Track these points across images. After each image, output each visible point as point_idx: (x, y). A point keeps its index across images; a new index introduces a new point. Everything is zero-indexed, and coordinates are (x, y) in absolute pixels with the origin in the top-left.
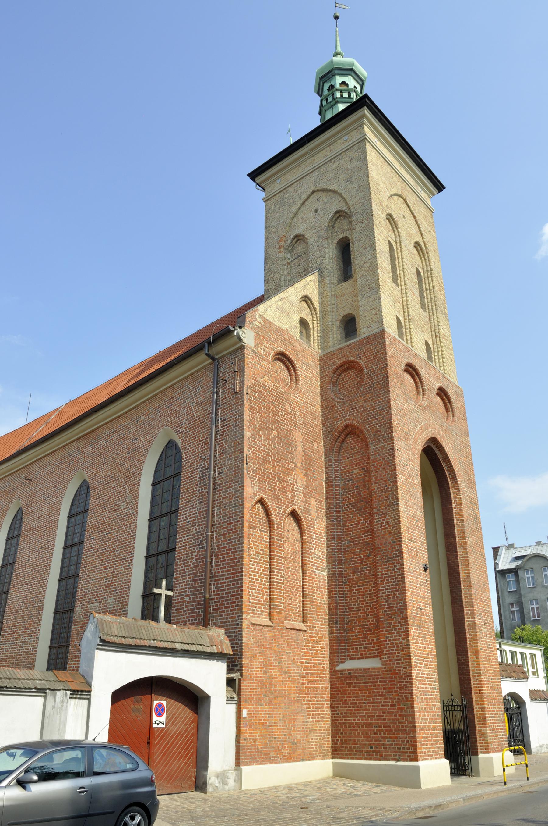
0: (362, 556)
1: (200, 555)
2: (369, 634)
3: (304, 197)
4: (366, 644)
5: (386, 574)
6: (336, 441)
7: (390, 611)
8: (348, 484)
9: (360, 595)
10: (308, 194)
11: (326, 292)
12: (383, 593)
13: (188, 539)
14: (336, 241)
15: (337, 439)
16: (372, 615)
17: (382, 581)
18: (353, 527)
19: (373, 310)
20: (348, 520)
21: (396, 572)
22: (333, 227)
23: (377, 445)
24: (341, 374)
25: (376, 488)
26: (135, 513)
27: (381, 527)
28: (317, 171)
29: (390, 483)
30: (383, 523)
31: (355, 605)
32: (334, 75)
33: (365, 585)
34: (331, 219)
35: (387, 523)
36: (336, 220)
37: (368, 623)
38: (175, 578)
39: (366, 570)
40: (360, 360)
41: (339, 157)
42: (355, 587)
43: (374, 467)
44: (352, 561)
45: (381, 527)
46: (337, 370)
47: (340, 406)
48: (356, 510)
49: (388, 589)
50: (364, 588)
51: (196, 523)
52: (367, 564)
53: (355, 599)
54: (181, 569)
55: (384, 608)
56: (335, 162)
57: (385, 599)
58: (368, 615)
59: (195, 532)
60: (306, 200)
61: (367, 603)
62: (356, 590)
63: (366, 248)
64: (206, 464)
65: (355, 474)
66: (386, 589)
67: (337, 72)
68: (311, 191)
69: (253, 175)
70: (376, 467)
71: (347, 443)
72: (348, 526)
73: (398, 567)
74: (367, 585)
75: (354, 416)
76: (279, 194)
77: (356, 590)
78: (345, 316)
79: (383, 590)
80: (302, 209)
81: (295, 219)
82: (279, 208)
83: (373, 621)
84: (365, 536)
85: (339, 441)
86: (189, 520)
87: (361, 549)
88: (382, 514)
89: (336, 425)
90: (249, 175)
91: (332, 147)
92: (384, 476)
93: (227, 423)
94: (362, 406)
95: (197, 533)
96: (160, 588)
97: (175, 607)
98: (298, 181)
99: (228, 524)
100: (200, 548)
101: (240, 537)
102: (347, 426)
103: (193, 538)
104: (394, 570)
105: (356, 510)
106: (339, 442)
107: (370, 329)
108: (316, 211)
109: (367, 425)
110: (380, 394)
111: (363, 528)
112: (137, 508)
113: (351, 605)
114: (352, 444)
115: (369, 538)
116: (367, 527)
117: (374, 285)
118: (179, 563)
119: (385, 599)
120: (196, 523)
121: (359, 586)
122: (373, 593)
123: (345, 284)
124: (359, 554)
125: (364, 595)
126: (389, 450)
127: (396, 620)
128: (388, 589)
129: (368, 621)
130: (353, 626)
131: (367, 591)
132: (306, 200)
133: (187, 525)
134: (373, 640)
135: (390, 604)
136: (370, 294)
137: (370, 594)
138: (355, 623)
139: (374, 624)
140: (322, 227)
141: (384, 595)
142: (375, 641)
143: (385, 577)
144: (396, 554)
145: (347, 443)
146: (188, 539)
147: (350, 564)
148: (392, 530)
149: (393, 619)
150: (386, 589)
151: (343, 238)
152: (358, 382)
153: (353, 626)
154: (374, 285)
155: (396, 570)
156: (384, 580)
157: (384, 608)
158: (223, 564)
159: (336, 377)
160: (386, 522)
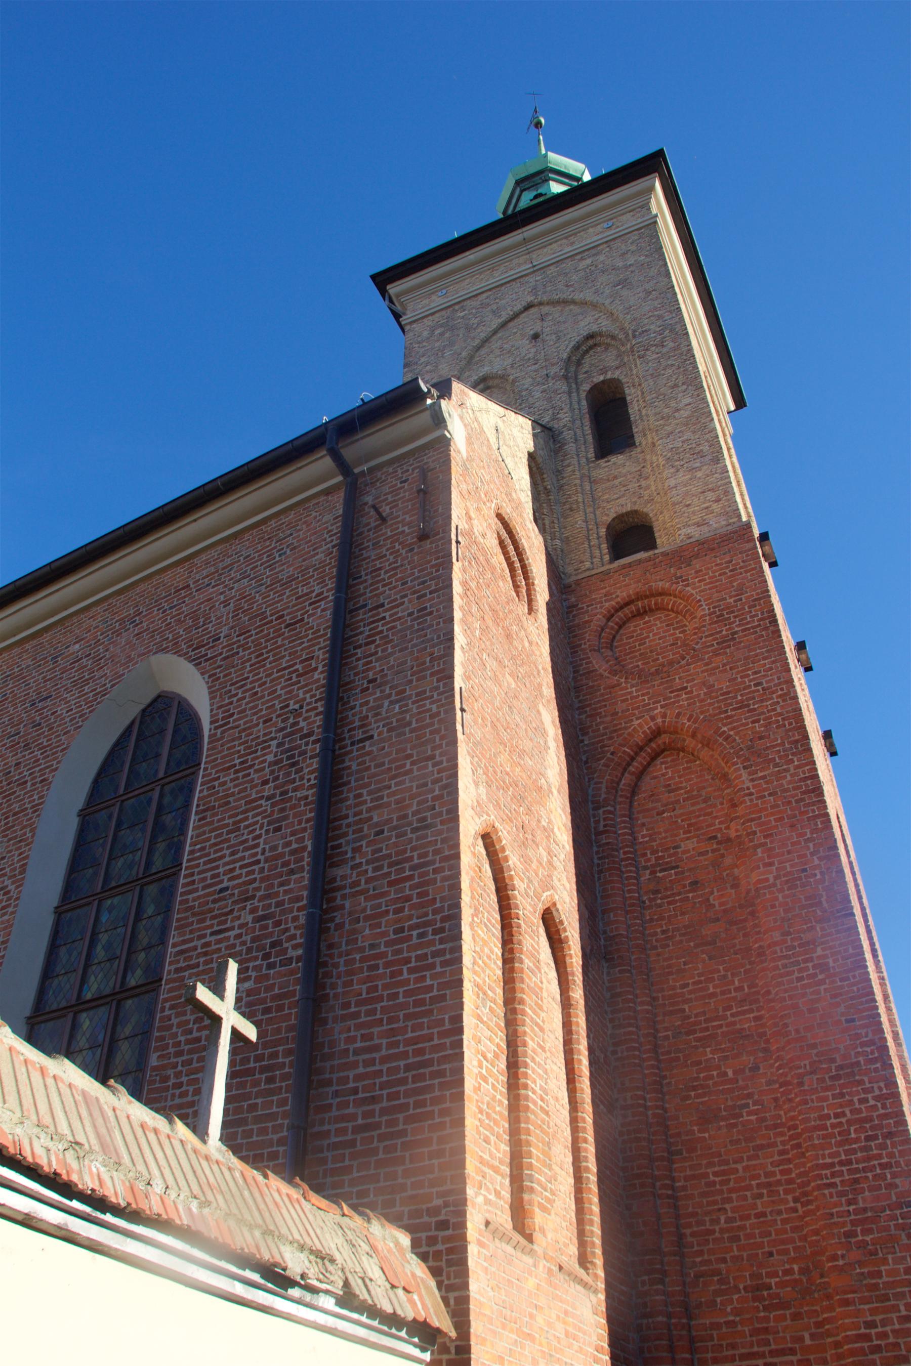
0: (730, 1073)
1: (270, 988)
2: (778, 1319)
3: (505, 316)
4: (772, 1353)
5: (837, 1116)
6: (625, 769)
7: (865, 1232)
8: (664, 877)
9: (730, 1191)
10: (519, 307)
11: (570, 469)
12: (833, 1175)
13: (219, 942)
14: (586, 387)
15: (629, 764)
16: (786, 1252)
17: (824, 1137)
18: (690, 992)
19: (710, 494)
20: (670, 973)
21: (874, 1108)
22: (579, 363)
23: (762, 770)
24: (624, 623)
25: (771, 877)
26: (12, 887)
27: (799, 979)
28: (539, 273)
29: (816, 862)
30: (807, 969)
31: (717, 1221)
32: (547, 180)
33: (749, 1158)
34: (577, 348)
35: (823, 967)
36: (587, 352)
37: (773, 1281)
38: (155, 1069)
39: (749, 1113)
40: (687, 585)
41: (593, 251)
42: (710, 1164)
43: (760, 825)
44: (694, 1088)
45: (799, 979)
46: (617, 611)
47: (632, 686)
48: (696, 946)
49: (849, 1162)
50: (746, 1168)
51: (258, 889)
52: (750, 1096)
53: (715, 1202)
54: (182, 1039)
55: (844, 1224)
56: (582, 259)
57: (841, 1194)
58: (771, 1254)
59: (250, 918)
60: (511, 319)
61: (763, 1214)
62: (716, 1174)
63: (676, 386)
64: (302, 724)
65: (684, 852)
66: (841, 1163)
67: (551, 175)
68: (524, 304)
69: (382, 280)
70: (764, 823)
71: (654, 778)
72: (673, 988)
73: (877, 1092)
74: (756, 1157)
75: (680, 707)
76: (443, 313)
77: (716, 1174)
78: (620, 518)
79: (832, 1165)
80: (499, 335)
81: (483, 351)
82: (442, 334)
83: (787, 1272)
84: (732, 1015)
85: (632, 769)
86: (225, 884)
87: (723, 1050)
88: (800, 946)
89: (626, 728)
90: (374, 277)
91: (572, 239)
92: (793, 844)
93: (387, 614)
94: (704, 683)
95: (257, 920)
96: (218, 990)
97: (284, 1077)
98: (490, 290)
99: (391, 884)
100: (271, 966)
101: (444, 919)
102: (657, 733)
103: (239, 936)
104: (863, 1101)
105: (696, 946)
106: (633, 773)
107: (705, 529)
108: (536, 337)
109: (725, 725)
110: (756, 655)
111: (723, 993)
112: (23, 871)
113: (700, 1223)
114: (672, 778)
115: (749, 1020)
116: (739, 989)
117: (705, 448)
118: (175, 1021)
119: (841, 1194)
120: (258, 889)
121: (727, 1163)
122: (779, 1183)
123: (617, 459)
124: (718, 1067)
125: (749, 1188)
126: (801, 780)
127: (895, 1262)
128: (849, 1162)
129: (771, 1275)
130: (717, 1293)
131: (757, 1177)
132: (511, 319)
133: (215, 901)
134: (801, 1339)
135: (865, 1210)
136: (698, 465)
137: (769, 1184)
138: (721, 1282)
139: (796, 1282)
140: (555, 361)
141: (837, 1180)
142: (808, 1342)
143: (833, 1126)
144: (864, 1054)
145: (654, 778)
146: (219, 942)
147: (688, 1097)
148: (842, 987)
149: (885, 1261)
150: (841, 1163)
151: (603, 382)
152: (677, 639)
153: (717, 1293)
154: (705, 448)
155: (872, 1102)
156: (832, 1135)
157: (844, 1224)
158: (369, 1013)
159: (612, 628)
160: (814, 967)
